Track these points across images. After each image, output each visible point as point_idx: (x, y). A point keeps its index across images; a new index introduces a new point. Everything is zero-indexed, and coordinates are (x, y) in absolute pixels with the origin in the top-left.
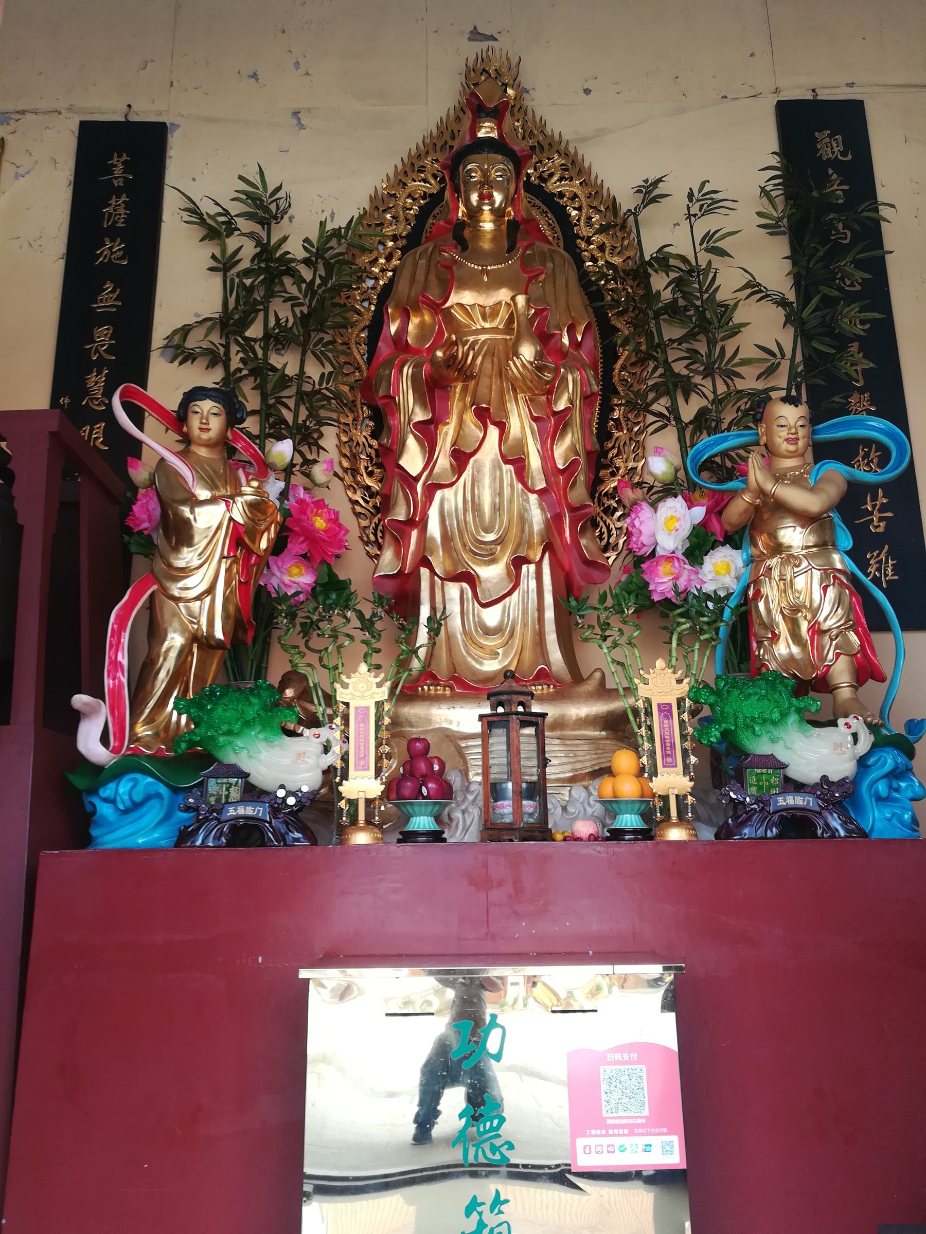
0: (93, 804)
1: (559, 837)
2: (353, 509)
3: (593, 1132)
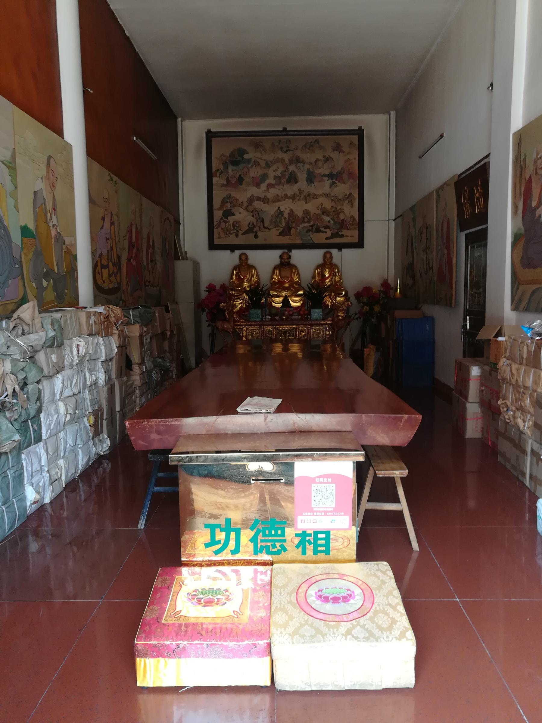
0: (31, 504)
1: (330, 588)
2: (42, 204)
3: (306, 514)
